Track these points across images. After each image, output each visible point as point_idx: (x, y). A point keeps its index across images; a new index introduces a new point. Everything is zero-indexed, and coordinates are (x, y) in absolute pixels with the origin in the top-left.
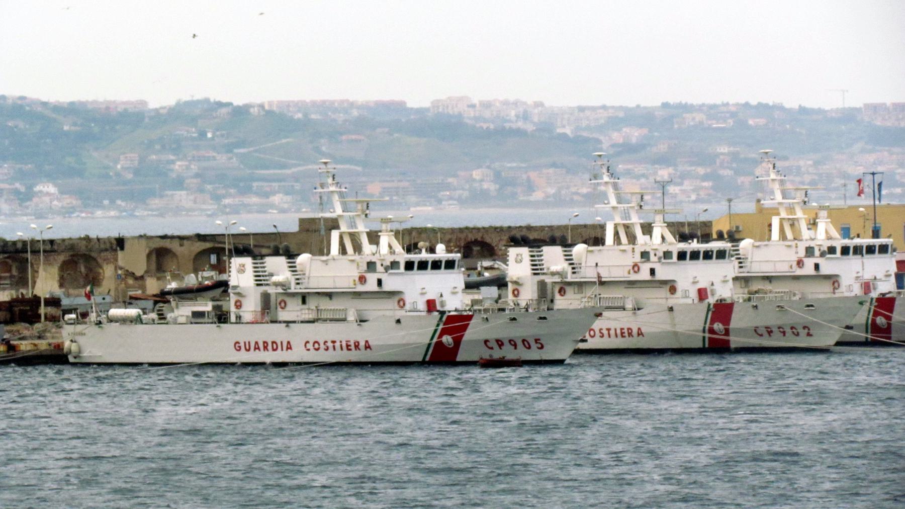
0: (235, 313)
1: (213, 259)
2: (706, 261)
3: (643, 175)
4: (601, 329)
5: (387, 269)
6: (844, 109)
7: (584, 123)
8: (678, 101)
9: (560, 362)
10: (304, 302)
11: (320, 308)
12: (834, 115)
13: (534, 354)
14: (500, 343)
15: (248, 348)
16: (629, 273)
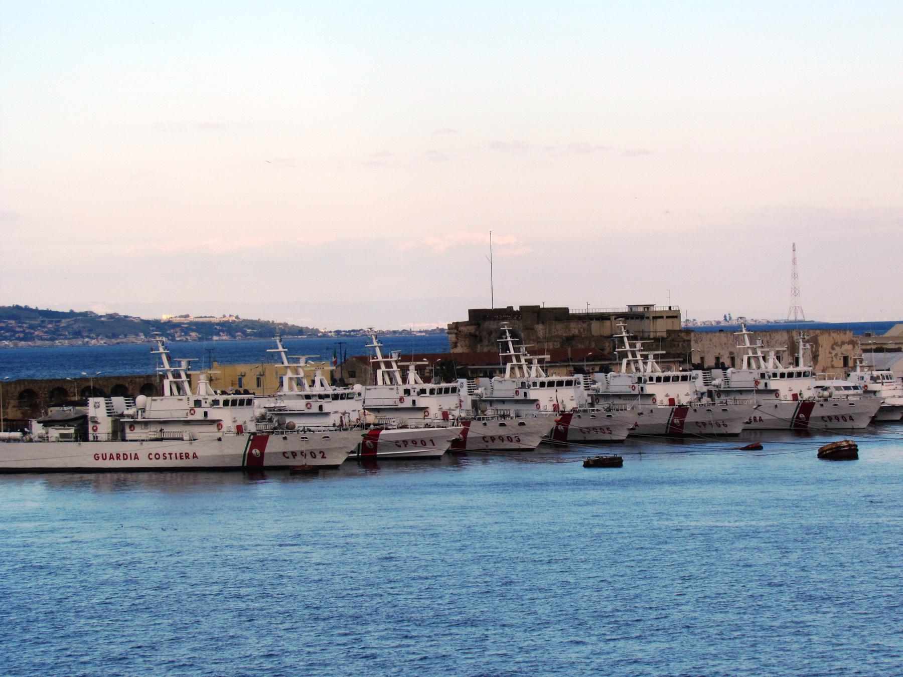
0: (93, 434)
2: (549, 388)
4: (164, 454)
5: (419, 394)
10: (883, 385)
15: (104, 457)
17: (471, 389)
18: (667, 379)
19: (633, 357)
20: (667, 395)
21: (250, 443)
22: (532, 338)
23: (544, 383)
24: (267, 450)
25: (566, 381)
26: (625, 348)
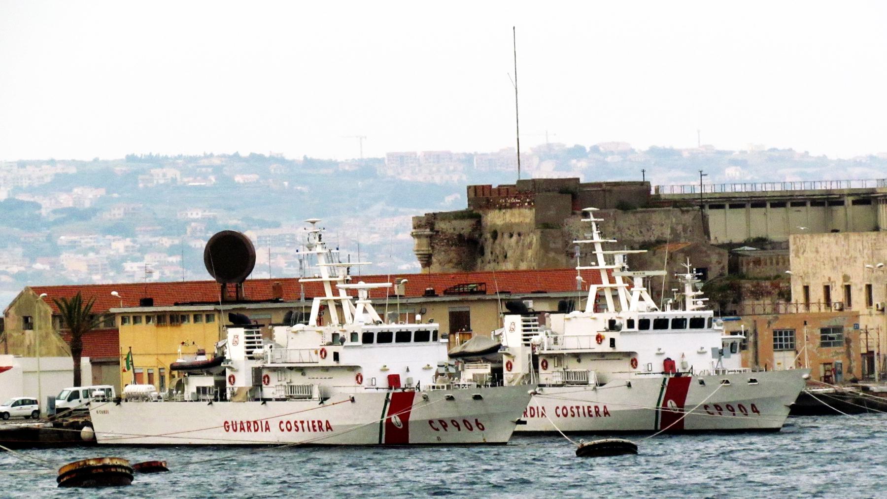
2: (694, 330)
3: (92, 249)
6: (361, 160)
7: (25, 183)
8: (147, 153)
12: (347, 168)
13: (476, 436)
15: (235, 428)
18: (661, 324)
19: (334, 295)
20: (384, 369)
22: (552, 245)
23: (648, 321)
25: (416, 333)
26: (597, 264)
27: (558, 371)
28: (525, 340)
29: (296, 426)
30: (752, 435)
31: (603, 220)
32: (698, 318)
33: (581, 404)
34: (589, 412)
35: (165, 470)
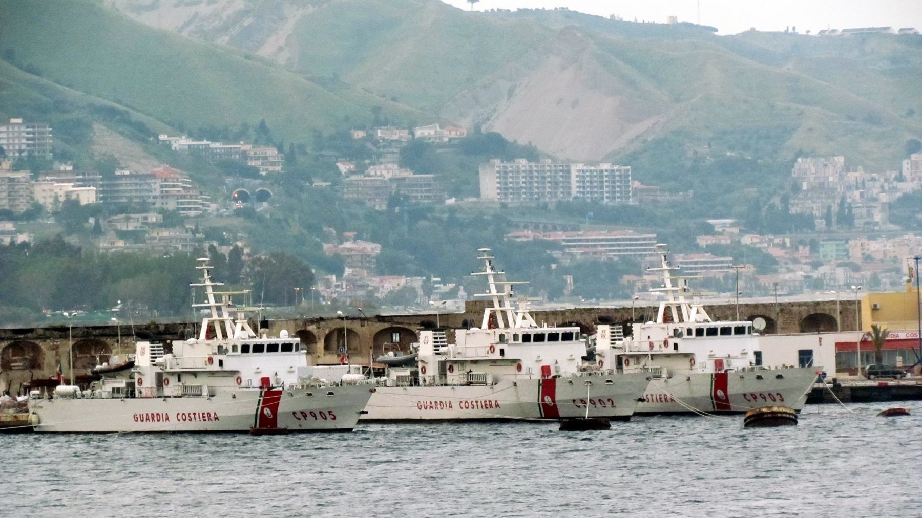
1: (396, 337)
2: (738, 336)
9: (349, 430)
11: (187, 385)
14: (754, 396)
16: (488, 353)
17: (437, 342)
18: (258, 348)
20: (711, 356)
21: (541, 387)
24: (280, 410)
26: (490, 292)
27: (178, 386)
28: (435, 350)
29: (190, 417)
30: (690, 417)
31: (213, 267)
32: (554, 334)
33: (446, 400)
34: (660, 399)
35: (907, 414)
